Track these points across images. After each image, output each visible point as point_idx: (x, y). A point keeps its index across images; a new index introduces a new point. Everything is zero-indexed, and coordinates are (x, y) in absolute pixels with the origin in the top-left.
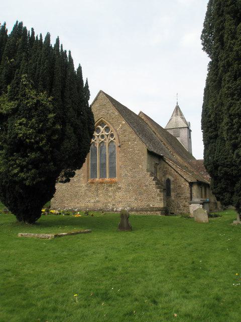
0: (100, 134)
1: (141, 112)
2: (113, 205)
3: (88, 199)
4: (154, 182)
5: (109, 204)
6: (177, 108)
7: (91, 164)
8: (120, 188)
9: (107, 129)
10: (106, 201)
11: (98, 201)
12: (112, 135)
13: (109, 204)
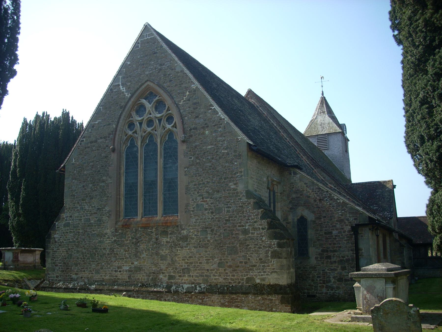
1: (250, 92)
2: (171, 277)
3: (116, 264)
4: (265, 223)
5: (161, 276)
6: (324, 101)
7: (126, 184)
8: (185, 238)
9: (160, 105)
11: (139, 269)
13: (161, 276)
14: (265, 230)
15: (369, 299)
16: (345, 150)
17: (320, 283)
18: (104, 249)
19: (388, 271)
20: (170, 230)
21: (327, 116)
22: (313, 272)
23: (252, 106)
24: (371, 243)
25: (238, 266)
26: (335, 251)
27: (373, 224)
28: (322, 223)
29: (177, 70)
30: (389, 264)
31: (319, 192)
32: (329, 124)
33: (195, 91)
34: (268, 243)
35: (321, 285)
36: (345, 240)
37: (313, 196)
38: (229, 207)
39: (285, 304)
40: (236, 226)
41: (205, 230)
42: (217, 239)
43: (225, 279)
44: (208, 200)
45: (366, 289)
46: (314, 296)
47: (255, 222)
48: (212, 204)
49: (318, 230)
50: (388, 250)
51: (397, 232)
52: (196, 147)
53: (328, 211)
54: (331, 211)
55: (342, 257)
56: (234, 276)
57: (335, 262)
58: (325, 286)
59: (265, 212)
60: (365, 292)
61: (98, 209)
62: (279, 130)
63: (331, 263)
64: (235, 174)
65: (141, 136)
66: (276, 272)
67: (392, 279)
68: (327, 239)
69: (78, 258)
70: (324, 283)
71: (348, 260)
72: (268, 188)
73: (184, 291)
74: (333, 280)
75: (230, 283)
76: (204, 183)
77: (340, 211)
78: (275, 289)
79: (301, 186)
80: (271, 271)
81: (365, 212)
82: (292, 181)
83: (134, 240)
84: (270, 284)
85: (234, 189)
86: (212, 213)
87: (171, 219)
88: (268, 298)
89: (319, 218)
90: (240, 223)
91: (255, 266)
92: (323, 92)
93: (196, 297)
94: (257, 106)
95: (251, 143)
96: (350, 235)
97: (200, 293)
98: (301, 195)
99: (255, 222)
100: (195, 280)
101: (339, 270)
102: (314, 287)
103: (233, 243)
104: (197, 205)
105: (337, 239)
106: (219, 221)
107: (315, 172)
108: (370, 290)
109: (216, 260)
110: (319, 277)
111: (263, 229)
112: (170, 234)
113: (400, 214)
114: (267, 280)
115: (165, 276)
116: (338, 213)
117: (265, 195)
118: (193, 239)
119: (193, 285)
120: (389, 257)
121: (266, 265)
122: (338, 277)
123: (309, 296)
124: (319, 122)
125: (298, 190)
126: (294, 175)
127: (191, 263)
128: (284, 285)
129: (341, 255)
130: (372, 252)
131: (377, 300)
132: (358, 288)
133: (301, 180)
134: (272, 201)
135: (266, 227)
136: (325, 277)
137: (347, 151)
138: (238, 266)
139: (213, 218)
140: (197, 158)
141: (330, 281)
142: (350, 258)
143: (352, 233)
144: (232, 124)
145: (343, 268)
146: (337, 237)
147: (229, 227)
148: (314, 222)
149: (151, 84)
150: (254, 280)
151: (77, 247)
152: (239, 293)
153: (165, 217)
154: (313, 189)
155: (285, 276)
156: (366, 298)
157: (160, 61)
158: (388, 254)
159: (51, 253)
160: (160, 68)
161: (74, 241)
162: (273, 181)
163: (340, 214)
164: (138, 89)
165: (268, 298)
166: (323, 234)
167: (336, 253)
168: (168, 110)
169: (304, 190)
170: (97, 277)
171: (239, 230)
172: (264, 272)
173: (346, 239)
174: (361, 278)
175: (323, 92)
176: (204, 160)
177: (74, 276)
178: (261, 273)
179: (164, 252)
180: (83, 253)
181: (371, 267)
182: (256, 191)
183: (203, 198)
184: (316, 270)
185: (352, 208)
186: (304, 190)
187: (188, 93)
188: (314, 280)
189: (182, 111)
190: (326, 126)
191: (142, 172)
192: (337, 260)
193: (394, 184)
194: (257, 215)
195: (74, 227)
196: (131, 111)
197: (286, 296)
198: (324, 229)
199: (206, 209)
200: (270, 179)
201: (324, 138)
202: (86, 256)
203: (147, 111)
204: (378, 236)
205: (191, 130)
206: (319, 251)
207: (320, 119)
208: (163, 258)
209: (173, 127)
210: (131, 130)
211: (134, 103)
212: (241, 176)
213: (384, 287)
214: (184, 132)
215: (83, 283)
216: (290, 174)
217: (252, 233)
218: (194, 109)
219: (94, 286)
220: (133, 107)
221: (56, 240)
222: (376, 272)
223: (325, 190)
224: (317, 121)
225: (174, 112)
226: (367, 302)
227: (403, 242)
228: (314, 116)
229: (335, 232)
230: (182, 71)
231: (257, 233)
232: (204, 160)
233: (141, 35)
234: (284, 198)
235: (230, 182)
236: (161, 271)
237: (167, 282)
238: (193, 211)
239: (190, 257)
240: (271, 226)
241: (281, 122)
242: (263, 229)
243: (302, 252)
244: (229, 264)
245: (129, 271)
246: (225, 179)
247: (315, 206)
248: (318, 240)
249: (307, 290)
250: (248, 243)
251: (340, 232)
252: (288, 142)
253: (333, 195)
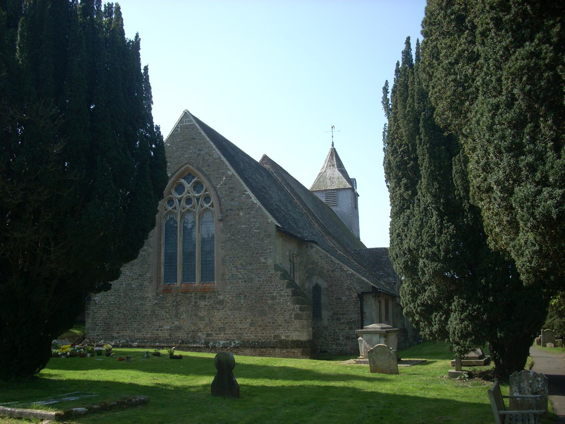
0: (184, 195)
1: (265, 158)
2: (208, 335)
3: (158, 324)
4: (289, 291)
5: (200, 334)
6: (334, 153)
7: (166, 253)
8: (221, 302)
9: (198, 186)
10: (193, 328)
11: (179, 328)
12: (207, 199)
13: (200, 334)
18: (146, 310)
20: (207, 295)
21: (337, 170)
23: (269, 175)
25: (267, 326)
26: (343, 314)
27: (375, 292)
29: (215, 157)
32: (338, 178)
33: (231, 177)
38: (259, 278)
40: (265, 293)
41: (239, 296)
42: (249, 303)
43: (256, 336)
44: (242, 271)
45: (366, 341)
46: (326, 352)
47: (281, 290)
48: (245, 274)
50: (390, 314)
52: (231, 225)
56: (263, 333)
57: (344, 323)
60: (366, 344)
61: (140, 275)
63: (341, 324)
64: (265, 250)
65: (181, 213)
67: (385, 334)
69: (119, 319)
71: (354, 322)
72: (290, 261)
73: (221, 346)
74: (341, 338)
75: (260, 339)
76: (238, 257)
78: (297, 344)
81: (369, 282)
82: (309, 253)
83: (175, 303)
85: (264, 263)
86: (245, 282)
87: (209, 285)
90: (269, 290)
91: (281, 325)
92: (333, 143)
93: (231, 351)
95: (279, 225)
97: (234, 347)
98: (316, 266)
99: (281, 290)
100: (230, 337)
103: (263, 307)
104: (232, 275)
106: (251, 289)
108: (369, 342)
109: (248, 320)
110: (329, 336)
111: (287, 296)
112: (208, 298)
114: (290, 337)
115: (204, 334)
117: (287, 266)
118: (229, 303)
119: (228, 342)
120: (391, 320)
125: (314, 262)
127: (227, 323)
130: (375, 315)
132: (361, 341)
134: (292, 271)
137: (356, 207)
138: (267, 326)
139: (246, 286)
140: (233, 235)
141: (339, 339)
144: (263, 208)
145: (351, 329)
147: (260, 294)
149: (191, 167)
150: (280, 336)
151: (119, 308)
152: (268, 347)
153: (203, 284)
154: (327, 261)
155: (305, 334)
157: (198, 146)
159: (92, 314)
160: (198, 152)
161: (115, 304)
162: (293, 254)
164: (178, 170)
168: (206, 191)
170: (138, 335)
171: (268, 297)
172: (288, 330)
175: (333, 143)
176: (239, 237)
177: (115, 335)
179: (202, 313)
180: (124, 314)
182: (281, 264)
183: (237, 269)
185: (359, 279)
187: (224, 178)
189: (219, 193)
191: (181, 244)
195: (115, 291)
196: (171, 189)
197: (306, 349)
199: (240, 279)
201: (333, 193)
202: (128, 317)
203: (186, 190)
204: (379, 302)
205: (227, 210)
207: (329, 173)
208: (202, 319)
209: (210, 206)
210: (171, 206)
211: (174, 182)
212: (271, 252)
214: (221, 213)
215: (124, 341)
216: (308, 247)
217: (279, 299)
218: (231, 192)
219: (136, 344)
220: (173, 185)
221: (97, 302)
224: (326, 175)
225: (212, 193)
228: (323, 168)
229: (344, 298)
230: (220, 158)
232: (239, 237)
233: (181, 121)
235: (261, 256)
236: (199, 330)
237: (205, 339)
238: (228, 280)
239: (226, 318)
240: (294, 294)
241: (297, 190)
242: (287, 296)
243: (316, 315)
244: (259, 324)
245: (170, 330)
246: (257, 254)
248: (330, 304)
250: (275, 307)
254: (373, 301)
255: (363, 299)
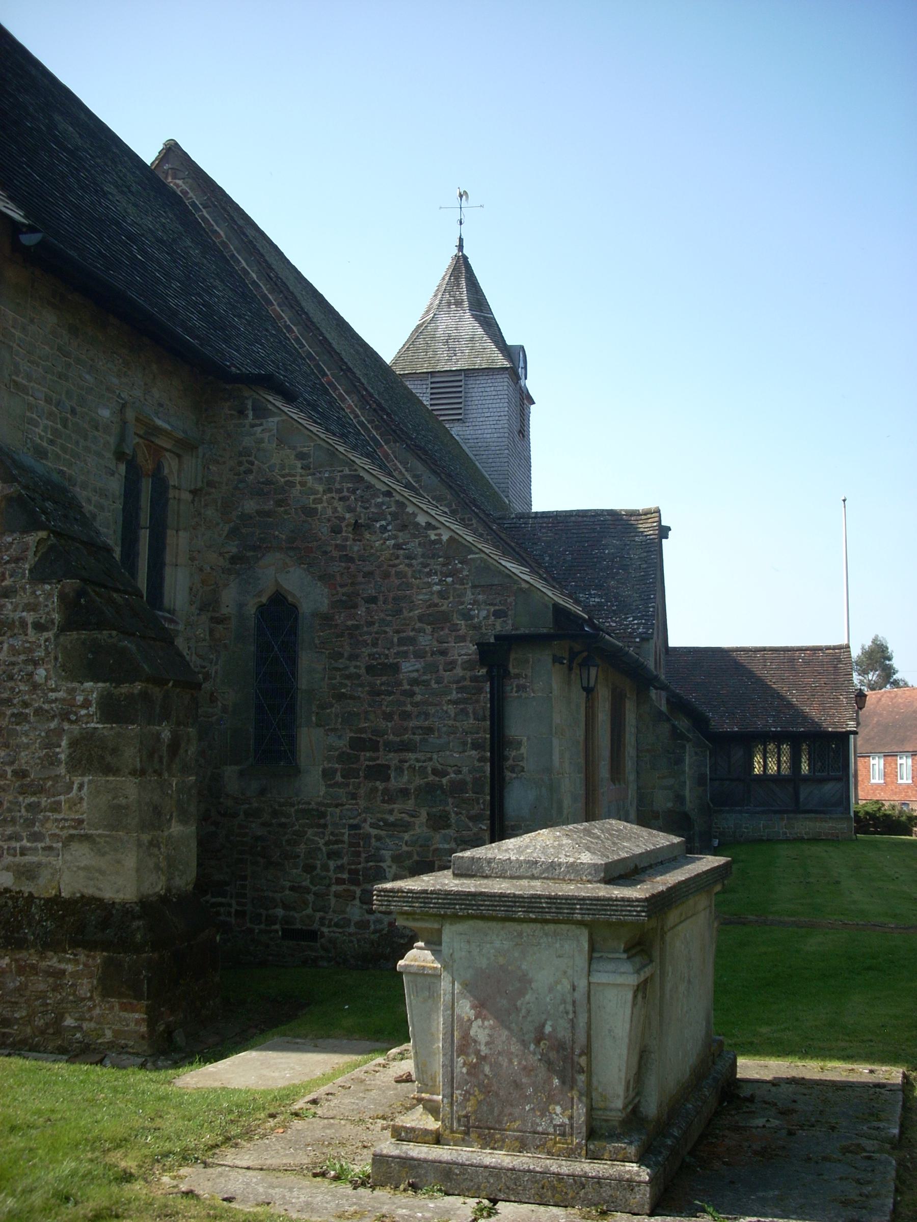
1: (172, 150)
4: (48, 598)
6: (462, 269)
14: (50, 634)
15: (484, 1050)
16: (516, 428)
17: (340, 882)
19: (610, 880)
21: (468, 315)
22: (310, 832)
23: (174, 200)
24: (557, 719)
28: (357, 627)
30: (621, 825)
31: (354, 492)
32: (472, 339)
34: (61, 694)
35: (340, 888)
36: (450, 702)
37: (329, 512)
39: (120, 995)
46: (313, 935)
49: (341, 655)
50: (630, 751)
51: (664, 688)
53: (386, 575)
54: (399, 575)
55: (435, 772)
57: (405, 793)
58: (358, 893)
59: (52, 548)
60: (465, 1009)
62: (264, 297)
63: (389, 797)
66: (87, 838)
68: (375, 693)
70: (357, 883)
71: (458, 787)
72: (120, 456)
77: (436, 579)
78: (79, 922)
79: (283, 467)
80: (64, 833)
82: (247, 442)
84: (58, 895)
88: (44, 964)
89: (348, 604)
92: (461, 240)
94: (194, 204)
96: (475, 679)
98: (279, 503)
101: (420, 827)
102: (311, 898)
105: (418, 698)
107: (387, 455)
108: (494, 992)
110: (331, 855)
111: (39, 627)
113: (676, 639)
114: (45, 876)
116: (430, 585)
121: (44, 801)
122: (416, 858)
123: (290, 934)
124: (440, 332)
125: (268, 482)
126: (256, 417)
128: (124, 904)
129: (429, 766)
130: (564, 759)
131: (533, 1060)
132: (426, 977)
133: (281, 441)
135: (56, 616)
136: (358, 854)
137: (522, 431)
142: (469, 778)
143: (483, 671)
145: (439, 822)
146: (416, 689)
148: (326, 619)
154: (331, 480)
155: (130, 861)
156: (465, 1045)
158: (629, 765)
163: (436, 588)
165: (44, 964)
166: (363, 671)
167: (411, 756)
169: (291, 484)
172: (36, 837)
173: (454, 696)
174: (444, 917)
175: (461, 240)
178: (18, 838)
181: (510, 849)
182: (41, 453)
184: (325, 826)
185: (486, 568)
186: (291, 484)
188: (314, 868)
190: (466, 348)
192: (412, 787)
193: (663, 524)
194: (17, 560)
198: (366, 651)
200: (130, 415)
204: (589, 691)
206: (342, 743)
207: (445, 323)
213: (582, 984)
216: (242, 413)
222: (537, 887)
223: (379, 486)
224: (436, 330)
226: (473, 1070)
227: (683, 724)
228: (427, 312)
229: (409, 667)
231: (12, 647)
234: (210, 512)
240: (77, 614)
241: (309, 306)
247: (336, 554)
248: (341, 697)
249: (286, 907)
251: (432, 668)
252: (297, 339)
253: (410, 509)
254: (556, 685)
255: (506, 674)
